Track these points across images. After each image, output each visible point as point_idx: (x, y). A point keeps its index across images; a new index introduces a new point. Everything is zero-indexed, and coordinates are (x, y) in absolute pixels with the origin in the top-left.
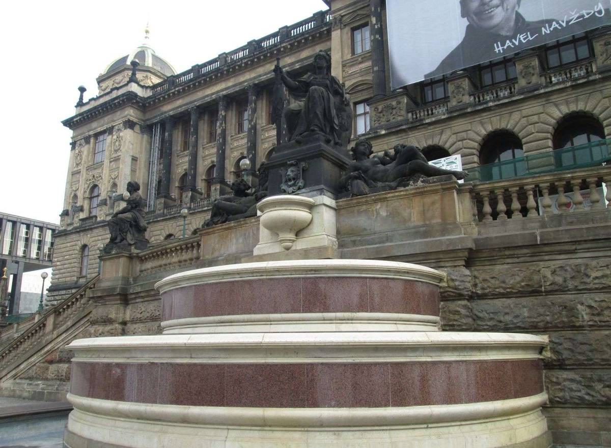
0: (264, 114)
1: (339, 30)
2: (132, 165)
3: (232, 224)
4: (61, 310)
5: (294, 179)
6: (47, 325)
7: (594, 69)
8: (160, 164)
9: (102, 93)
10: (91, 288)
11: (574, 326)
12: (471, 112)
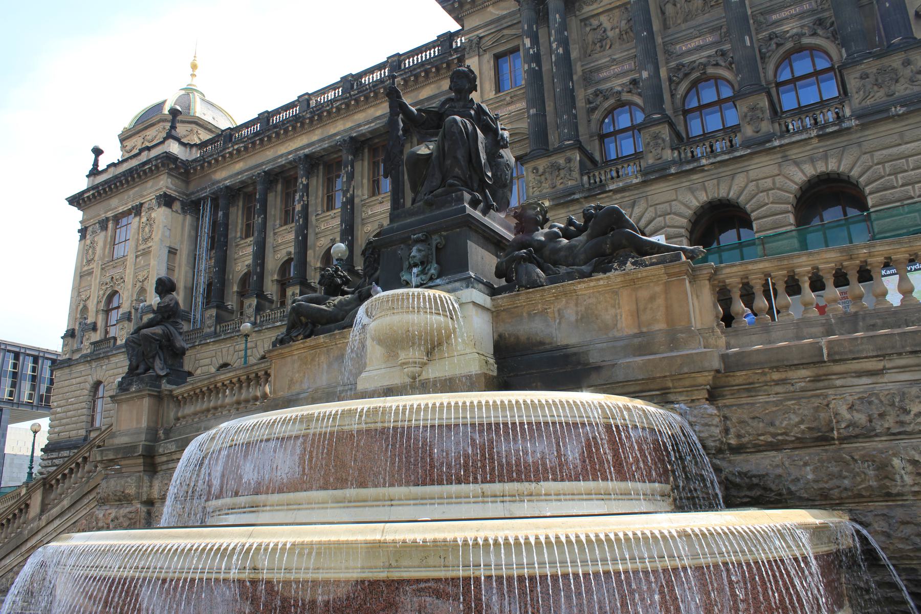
0: (365, 181)
1: (476, 58)
2: (168, 261)
3: (322, 339)
4: (53, 482)
5: (422, 263)
6: (32, 505)
7: (848, 112)
8: (210, 258)
9: (127, 155)
10: (99, 447)
11: (889, 494)
12: (677, 173)
